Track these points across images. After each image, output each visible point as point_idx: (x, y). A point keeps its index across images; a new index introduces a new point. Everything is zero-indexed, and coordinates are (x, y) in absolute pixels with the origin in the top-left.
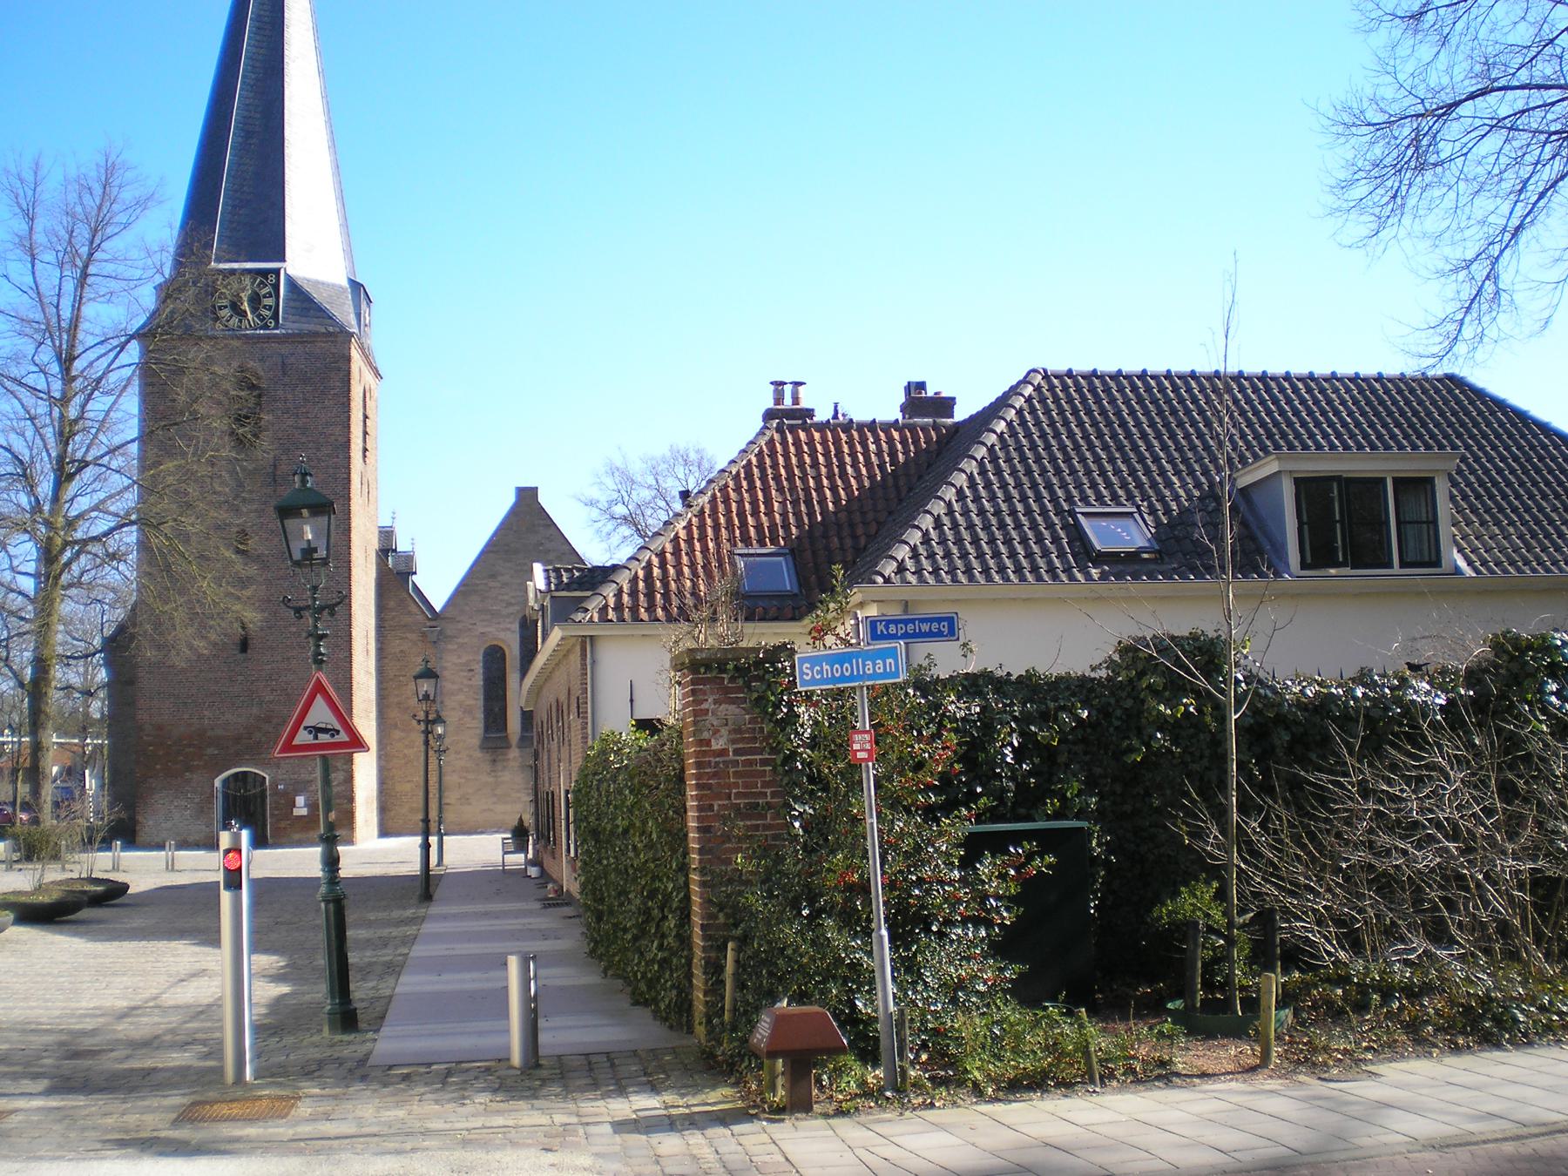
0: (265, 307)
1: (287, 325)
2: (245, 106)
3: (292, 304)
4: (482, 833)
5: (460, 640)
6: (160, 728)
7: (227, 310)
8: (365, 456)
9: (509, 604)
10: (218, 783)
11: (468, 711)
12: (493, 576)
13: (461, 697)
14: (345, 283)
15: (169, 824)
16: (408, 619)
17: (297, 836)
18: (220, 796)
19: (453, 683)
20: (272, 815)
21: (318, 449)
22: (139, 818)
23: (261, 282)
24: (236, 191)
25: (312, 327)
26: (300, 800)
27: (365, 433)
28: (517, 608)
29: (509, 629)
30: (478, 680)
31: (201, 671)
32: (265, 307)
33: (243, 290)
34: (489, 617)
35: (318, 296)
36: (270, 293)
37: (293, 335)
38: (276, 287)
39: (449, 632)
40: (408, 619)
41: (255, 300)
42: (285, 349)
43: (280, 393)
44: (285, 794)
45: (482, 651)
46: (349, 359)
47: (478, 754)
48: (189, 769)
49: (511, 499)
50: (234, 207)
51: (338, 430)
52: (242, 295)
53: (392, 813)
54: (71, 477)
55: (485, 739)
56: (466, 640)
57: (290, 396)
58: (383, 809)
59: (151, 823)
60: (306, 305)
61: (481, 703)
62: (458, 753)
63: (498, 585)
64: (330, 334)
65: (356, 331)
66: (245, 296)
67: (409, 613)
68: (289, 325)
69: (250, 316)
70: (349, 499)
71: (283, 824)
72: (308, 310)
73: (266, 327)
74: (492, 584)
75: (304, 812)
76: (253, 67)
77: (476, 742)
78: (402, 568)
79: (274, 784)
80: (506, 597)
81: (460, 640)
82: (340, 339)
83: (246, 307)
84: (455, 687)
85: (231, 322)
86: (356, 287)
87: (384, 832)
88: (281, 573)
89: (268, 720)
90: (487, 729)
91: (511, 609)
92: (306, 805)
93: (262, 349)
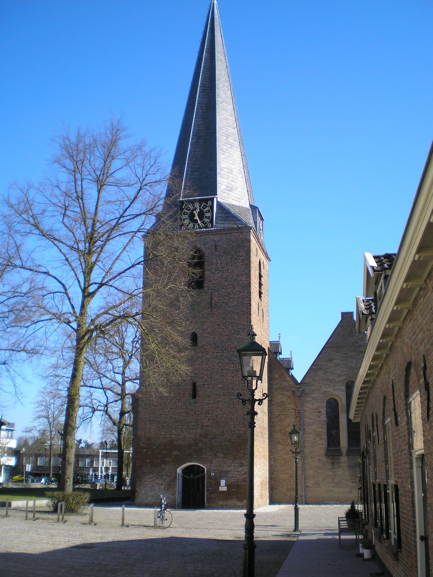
0: (206, 217)
1: (217, 225)
2: (196, 125)
3: (220, 215)
4: (327, 504)
5: (313, 395)
6: (149, 439)
7: (187, 220)
8: (260, 297)
9: (339, 376)
10: (179, 471)
11: (318, 434)
12: (331, 360)
13: (314, 427)
14: (248, 206)
15: (153, 493)
16: (285, 384)
17: (221, 503)
18: (181, 478)
19: (310, 419)
20: (207, 490)
21: (234, 288)
22: (138, 489)
23: (205, 205)
24: (192, 164)
25: (230, 226)
26: (223, 482)
27: (260, 285)
28: (344, 377)
29: (340, 389)
30: (324, 417)
31: (172, 408)
32: (206, 217)
33: (195, 210)
34: (329, 383)
35: (233, 211)
36: (209, 210)
37: (220, 230)
38: (212, 207)
39: (307, 391)
40: (285, 384)
41: (201, 215)
42: (217, 238)
43: (214, 260)
44: (215, 478)
45: (325, 402)
46: (249, 241)
47: (324, 459)
48: (165, 463)
49: (339, 319)
50: (192, 172)
51: (244, 278)
52: (195, 212)
53: (278, 491)
54: (92, 294)
55: (328, 450)
56: (317, 395)
57: (219, 262)
58: (272, 489)
59: (143, 492)
60: (227, 215)
61: (325, 430)
62: (312, 458)
63: (333, 365)
64: (239, 228)
65: (254, 226)
66: (196, 213)
67: (286, 381)
68: (219, 225)
69: (199, 222)
70: (250, 314)
71: (213, 496)
72: (229, 217)
73: (206, 227)
74: (330, 365)
75: (225, 489)
76: (201, 107)
77: (323, 452)
78: (286, 366)
79: (209, 472)
80: (338, 372)
81: (313, 395)
82: (245, 231)
83: (197, 217)
84: (311, 421)
85: (189, 226)
86: (254, 208)
87: (272, 502)
88: (214, 355)
89: (206, 436)
90: (329, 444)
91: (342, 378)
92: (226, 485)
93: (205, 239)
